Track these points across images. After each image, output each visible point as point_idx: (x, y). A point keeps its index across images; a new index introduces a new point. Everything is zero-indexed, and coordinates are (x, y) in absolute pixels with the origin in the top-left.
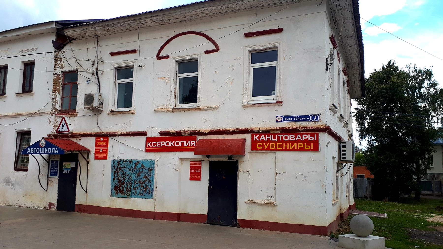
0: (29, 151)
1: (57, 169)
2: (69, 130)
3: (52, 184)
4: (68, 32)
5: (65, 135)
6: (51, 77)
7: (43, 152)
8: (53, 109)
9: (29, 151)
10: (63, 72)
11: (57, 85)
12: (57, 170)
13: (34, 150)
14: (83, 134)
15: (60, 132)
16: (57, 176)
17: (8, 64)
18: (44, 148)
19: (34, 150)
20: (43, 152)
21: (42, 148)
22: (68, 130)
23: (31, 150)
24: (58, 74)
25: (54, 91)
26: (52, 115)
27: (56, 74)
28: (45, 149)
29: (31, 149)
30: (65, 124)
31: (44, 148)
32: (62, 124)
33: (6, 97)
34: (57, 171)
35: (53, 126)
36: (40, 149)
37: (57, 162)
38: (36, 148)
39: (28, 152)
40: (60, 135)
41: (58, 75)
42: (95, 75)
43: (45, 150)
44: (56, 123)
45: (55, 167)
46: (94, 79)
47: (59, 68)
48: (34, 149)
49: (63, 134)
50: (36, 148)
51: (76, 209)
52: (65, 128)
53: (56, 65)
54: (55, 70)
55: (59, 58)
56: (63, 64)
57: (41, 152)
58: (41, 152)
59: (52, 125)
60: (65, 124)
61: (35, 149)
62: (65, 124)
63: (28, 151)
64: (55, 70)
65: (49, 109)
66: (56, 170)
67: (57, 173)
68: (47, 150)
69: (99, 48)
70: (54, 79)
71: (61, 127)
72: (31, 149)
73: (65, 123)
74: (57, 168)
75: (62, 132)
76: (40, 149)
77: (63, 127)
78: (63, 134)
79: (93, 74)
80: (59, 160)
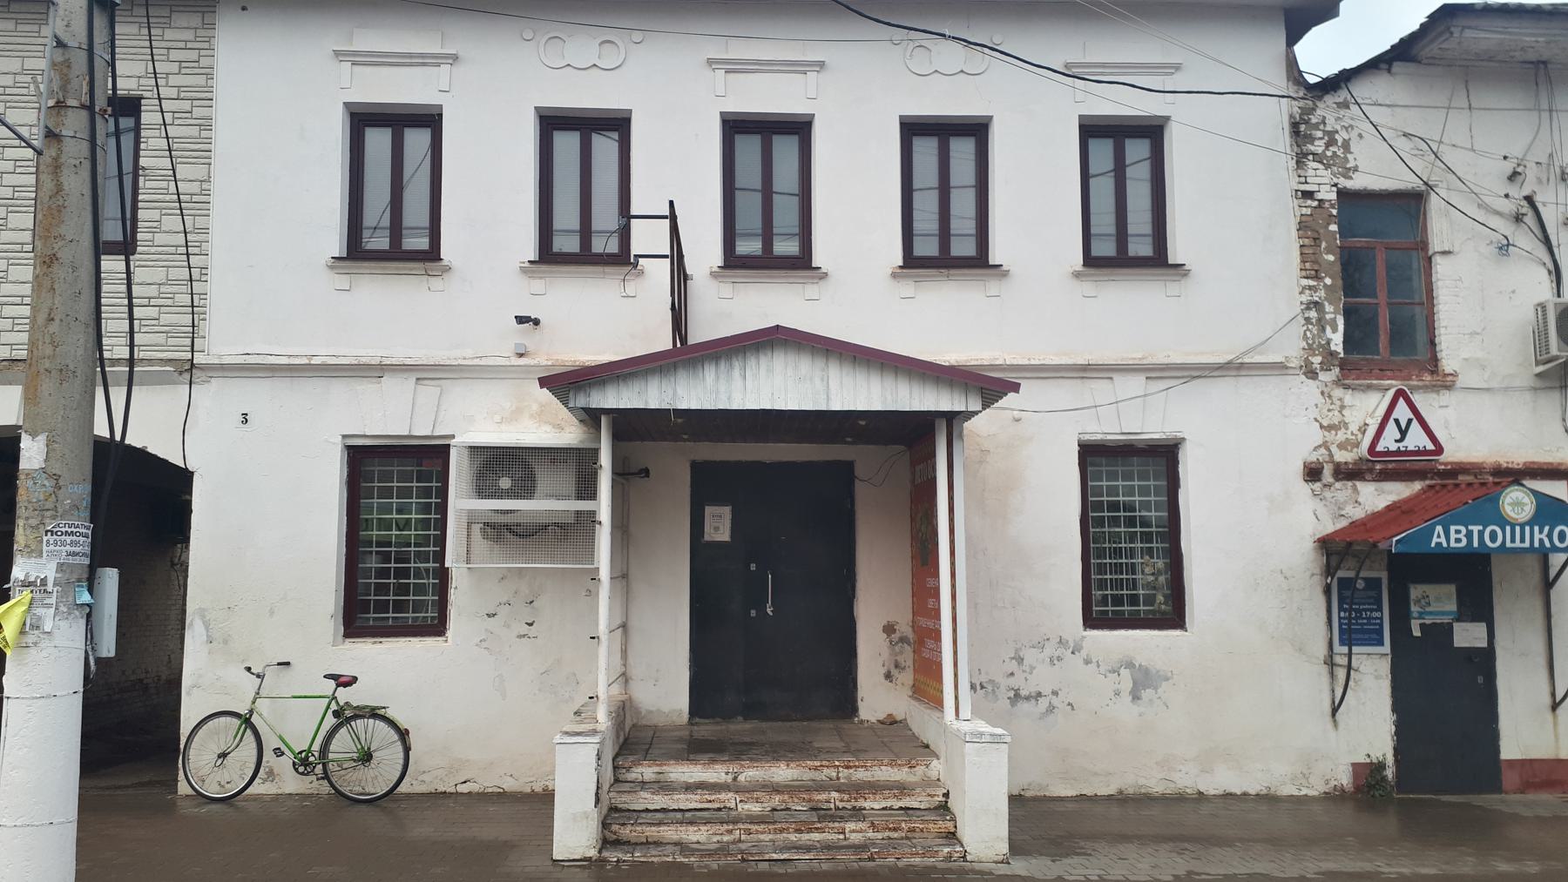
0: (1439, 536)
1: (1377, 614)
2: (1439, 450)
3: (1356, 682)
4: (1469, 28)
5: (1417, 466)
6: (1289, 214)
7: (1523, 540)
8: (1310, 349)
9: (1443, 540)
10: (1343, 194)
11: (1324, 245)
12: (1381, 619)
13: (1469, 535)
14: (1518, 464)
15: (1388, 453)
16: (1381, 644)
17: (990, 118)
18: (1527, 529)
19: (1469, 535)
20: (1523, 540)
21: (1518, 529)
22: (1433, 448)
23: (1453, 536)
24: (1319, 196)
25: (1304, 273)
26: (1311, 374)
27: (1308, 195)
28: (1536, 529)
29: (1453, 528)
30: (1415, 423)
31: (1527, 529)
32: (1397, 421)
33: (448, 269)
34: (1381, 625)
35: (1322, 427)
36: (1508, 528)
37: (1374, 584)
38: (1481, 528)
39: (1433, 545)
40: (1390, 466)
41: (1320, 201)
42: (1530, 219)
43: (1537, 536)
44: (1336, 413)
45: (1367, 607)
46: (1525, 240)
47: (1322, 172)
48: (1470, 527)
49: (1402, 466)
50: (1481, 528)
51: (1509, 779)
52: (1417, 439)
53: (1305, 155)
54: (1303, 180)
55: (1321, 127)
56: (1347, 160)
57: (1513, 541)
58: (1513, 541)
59: (1316, 420)
60: (1410, 421)
61: (1475, 529)
62: (1410, 421)
63: (1435, 540)
64: (1303, 180)
65: (1291, 348)
66: (1369, 619)
67: (1380, 632)
68: (1550, 536)
69: (1554, 114)
70: (1304, 219)
71: (1391, 431)
72: (1453, 528)
73: (1412, 416)
74: (1380, 609)
75: (1398, 453)
76: (1508, 528)
77: (1404, 434)
78: (1408, 465)
79: (1518, 218)
80: (1384, 575)
